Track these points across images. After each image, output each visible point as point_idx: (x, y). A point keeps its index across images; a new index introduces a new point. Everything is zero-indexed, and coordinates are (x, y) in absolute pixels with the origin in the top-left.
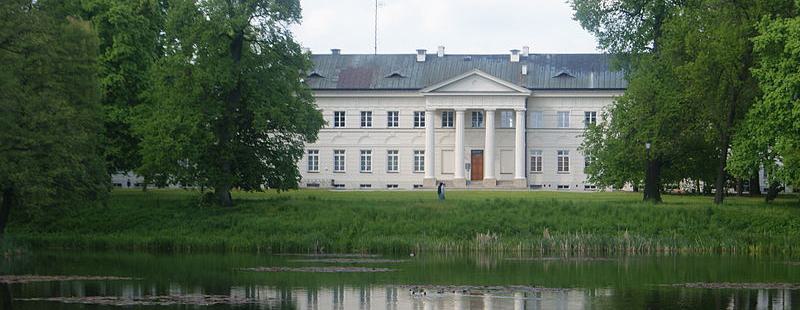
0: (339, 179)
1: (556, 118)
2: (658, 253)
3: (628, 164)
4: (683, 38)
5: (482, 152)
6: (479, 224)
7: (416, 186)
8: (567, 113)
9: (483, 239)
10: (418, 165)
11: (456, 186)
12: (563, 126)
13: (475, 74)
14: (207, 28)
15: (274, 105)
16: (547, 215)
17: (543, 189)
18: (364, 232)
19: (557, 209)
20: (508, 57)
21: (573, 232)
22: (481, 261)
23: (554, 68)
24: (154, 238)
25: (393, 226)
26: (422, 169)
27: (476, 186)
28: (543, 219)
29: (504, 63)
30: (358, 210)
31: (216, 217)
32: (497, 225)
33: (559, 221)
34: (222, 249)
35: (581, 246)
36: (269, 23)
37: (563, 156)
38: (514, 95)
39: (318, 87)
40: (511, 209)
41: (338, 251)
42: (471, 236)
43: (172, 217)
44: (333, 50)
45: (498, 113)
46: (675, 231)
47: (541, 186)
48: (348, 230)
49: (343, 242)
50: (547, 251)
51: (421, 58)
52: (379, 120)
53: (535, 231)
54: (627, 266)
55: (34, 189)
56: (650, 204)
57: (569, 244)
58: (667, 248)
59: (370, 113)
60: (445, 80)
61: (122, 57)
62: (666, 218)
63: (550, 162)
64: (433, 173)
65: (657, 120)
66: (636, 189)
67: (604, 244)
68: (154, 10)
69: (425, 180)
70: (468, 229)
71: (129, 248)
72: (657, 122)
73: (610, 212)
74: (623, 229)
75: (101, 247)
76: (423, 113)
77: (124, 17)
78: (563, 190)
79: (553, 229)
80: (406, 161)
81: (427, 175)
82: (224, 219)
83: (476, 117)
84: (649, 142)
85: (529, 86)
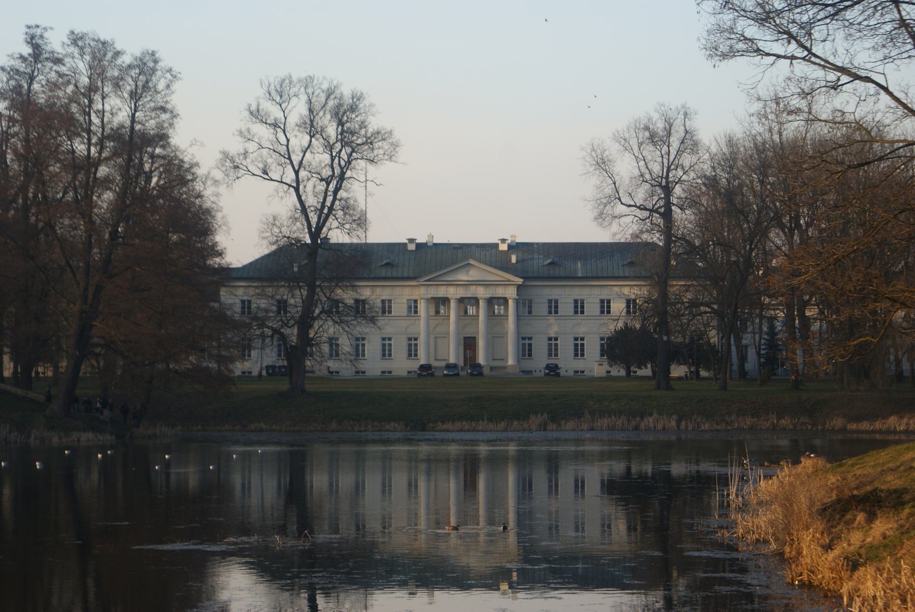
5: (474, 338)
10: (412, 352)
13: (469, 264)
20: (496, 245)
23: (541, 256)
26: (416, 355)
37: (527, 342)
38: (506, 284)
39: (399, 275)
59: (390, 301)
76: (416, 301)
77: (600, 188)
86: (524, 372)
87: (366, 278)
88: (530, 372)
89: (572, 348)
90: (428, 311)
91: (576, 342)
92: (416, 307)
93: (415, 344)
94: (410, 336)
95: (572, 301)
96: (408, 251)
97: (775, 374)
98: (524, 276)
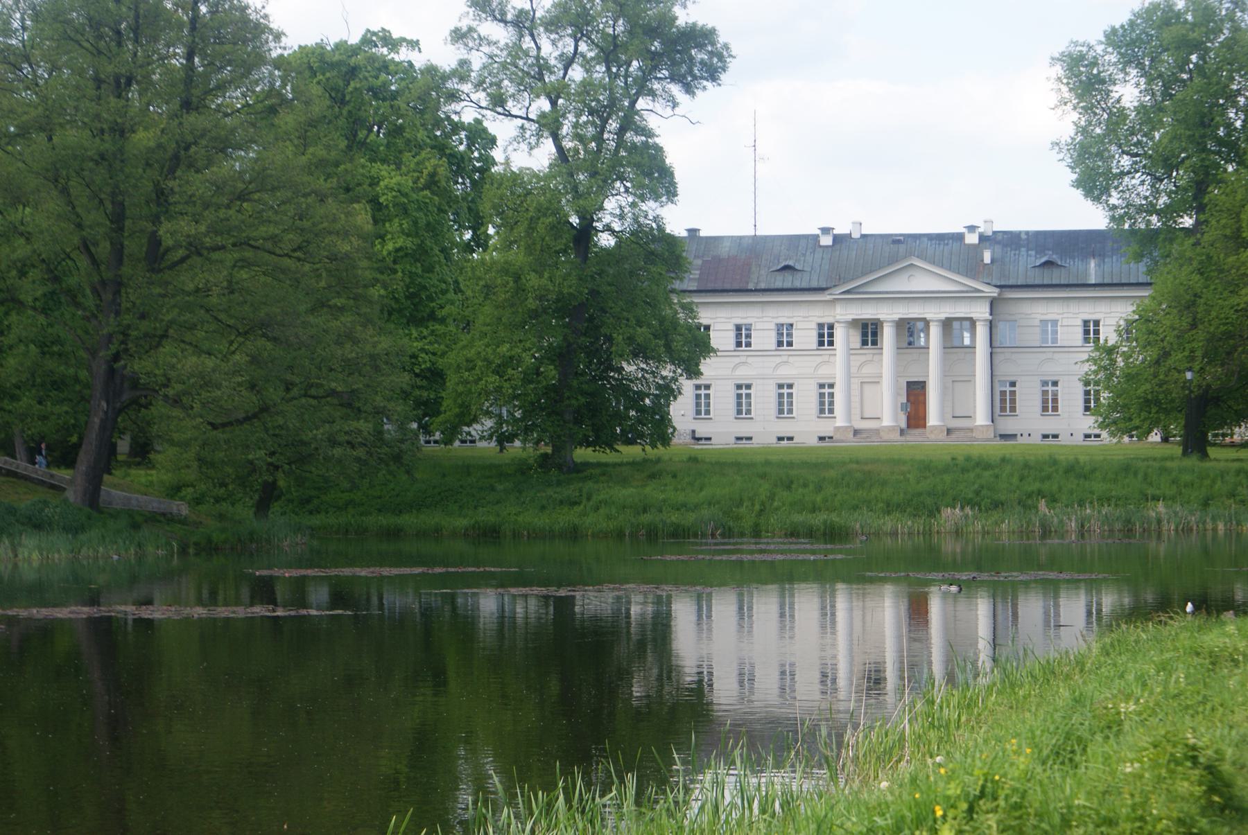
0: (702, 429)
1: (1038, 330)
2: (1210, 534)
3: (1157, 402)
4: (1238, 214)
6: (944, 494)
7: (821, 439)
8: (1055, 322)
9: (950, 515)
10: (825, 405)
11: (885, 436)
12: (1049, 342)
14: (545, 215)
15: (640, 323)
16: (1042, 480)
17: (1020, 440)
18: (777, 509)
19: (1057, 471)
20: (959, 237)
21: (1081, 504)
22: (949, 546)
23: (1033, 253)
24: (473, 521)
25: (819, 499)
26: (831, 411)
27: (915, 436)
28: (1037, 486)
29: (956, 246)
30: (763, 476)
31: (559, 489)
32: (971, 495)
33: (1060, 489)
34: (573, 534)
35: (1095, 526)
36: (633, 205)
39: (804, 285)
40: (991, 472)
41: (742, 535)
42: (934, 512)
43: (493, 489)
44: (689, 231)
45: (947, 324)
46: (1232, 501)
47: (1015, 436)
48: (753, 505)
49: (748, 523)
50: (1046, 532)
51: (826, 241)
52: (764, 338)
53: (1026, 503)
54: (1162, 554)
55: (337, 452)
56: (1193, 461)
57: (1076, 521)
58: (1221, 526)
60: (864, 274)
61: (400, 254)
62: (1219, 483)
63: (1028, 399)
64: (849, 418)
65: (1201, 335)
66: (1165, 440)
67: (1128, 521)
68: (443, 183)
69: (837, 429)
70: (929, 501)
71: (436, 533)
72: (1199, 340)
73: (1136, 474)
74: (1156, 498)
75: (394, 534)
76: (831, 327)
78: (1050, 441)
79: (1053, 500)
80: (805, 399)
81: (840, 421)
82: (569, 491)
83: (909, 330)
84: (1190, 369)
85: (995, 282)
86: (1004, 437)
87: (751, 291)
88: (1013, 436)
90: (848, 342)
92: (831, 335)
94: (822, 381)
95: (1080, 323)
96: (821, 246)
98: (1003, 283)
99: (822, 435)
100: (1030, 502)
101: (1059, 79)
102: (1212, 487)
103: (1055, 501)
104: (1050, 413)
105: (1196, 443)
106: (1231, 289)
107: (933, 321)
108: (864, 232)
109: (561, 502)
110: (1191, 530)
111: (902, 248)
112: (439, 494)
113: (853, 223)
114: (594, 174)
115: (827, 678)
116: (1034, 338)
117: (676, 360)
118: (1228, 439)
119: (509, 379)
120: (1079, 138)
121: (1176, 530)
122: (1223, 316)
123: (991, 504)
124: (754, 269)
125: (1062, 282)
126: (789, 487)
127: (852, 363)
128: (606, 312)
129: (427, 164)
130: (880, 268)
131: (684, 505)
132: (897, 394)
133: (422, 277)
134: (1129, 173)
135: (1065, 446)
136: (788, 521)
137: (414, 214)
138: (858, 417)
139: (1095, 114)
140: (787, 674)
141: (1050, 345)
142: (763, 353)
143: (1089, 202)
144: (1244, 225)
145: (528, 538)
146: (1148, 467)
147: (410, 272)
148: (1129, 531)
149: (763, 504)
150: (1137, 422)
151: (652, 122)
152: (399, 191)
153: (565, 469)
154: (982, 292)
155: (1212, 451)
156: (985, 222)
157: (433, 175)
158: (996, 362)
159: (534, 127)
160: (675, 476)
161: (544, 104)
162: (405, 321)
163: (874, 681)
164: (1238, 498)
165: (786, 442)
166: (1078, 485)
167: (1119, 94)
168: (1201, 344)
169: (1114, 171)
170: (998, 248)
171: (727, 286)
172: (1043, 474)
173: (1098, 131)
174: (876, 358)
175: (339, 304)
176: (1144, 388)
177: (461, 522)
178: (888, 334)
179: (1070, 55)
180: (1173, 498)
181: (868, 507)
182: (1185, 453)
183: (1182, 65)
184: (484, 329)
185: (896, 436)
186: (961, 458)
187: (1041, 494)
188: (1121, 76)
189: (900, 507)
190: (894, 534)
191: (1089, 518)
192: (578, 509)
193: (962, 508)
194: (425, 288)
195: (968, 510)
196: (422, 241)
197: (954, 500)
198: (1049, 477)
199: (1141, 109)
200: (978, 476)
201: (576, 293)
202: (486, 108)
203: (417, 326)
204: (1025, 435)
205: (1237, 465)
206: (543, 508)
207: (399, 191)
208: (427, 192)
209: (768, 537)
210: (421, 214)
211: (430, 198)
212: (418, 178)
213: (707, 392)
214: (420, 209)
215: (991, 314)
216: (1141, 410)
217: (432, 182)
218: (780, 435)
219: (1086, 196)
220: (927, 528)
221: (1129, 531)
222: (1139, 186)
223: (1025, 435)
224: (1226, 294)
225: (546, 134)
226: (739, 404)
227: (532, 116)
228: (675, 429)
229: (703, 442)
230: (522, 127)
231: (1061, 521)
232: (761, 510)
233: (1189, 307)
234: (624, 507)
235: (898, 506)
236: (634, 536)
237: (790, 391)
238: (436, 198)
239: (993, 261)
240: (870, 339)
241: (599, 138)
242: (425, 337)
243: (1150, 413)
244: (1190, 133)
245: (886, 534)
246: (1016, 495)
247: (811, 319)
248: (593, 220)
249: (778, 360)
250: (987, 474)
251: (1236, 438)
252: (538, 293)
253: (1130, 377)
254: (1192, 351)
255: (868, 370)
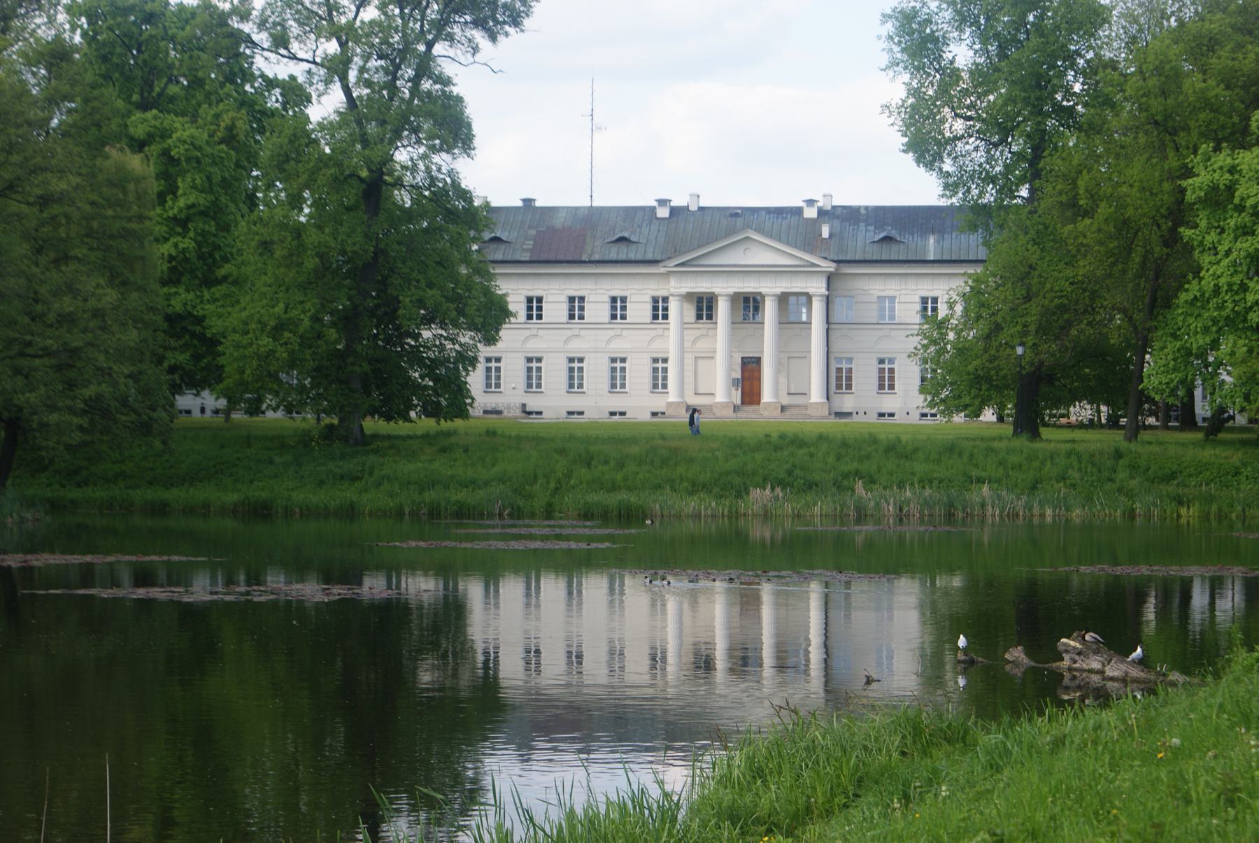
0: (533, 403)
1: (875, 306)
3: (989, 379)
4: (1074, 182)
7: (654, 414)
9: (759, 497)
10: (658, 381)
11: (719, 413)
12: (886, 319)
13: (748, 238)
14: (326, 166)
15: (430, 285)
16: (861, 460)
17: (855, 418)
20: (799, 211)
21: (901, 486)
22: (759, 532)
25: (619, 477)
26: (665, 386)
27: (749, 413)
29: (794, 219)
30: (562, 452)
31: (340, 463)
34: (350, 512)
35: (914, 509)
36: (424, 157)
37: (886, 366)
39: (639, 257)
41: (532, 515)
42: (741, 492)
43: (271, 462)
44: (524, 200)
45: (783, 299)
48: (548, 483)
49: (539, 503)
50: (861, 517)
51: (663, 213)
52: (597, 310)
53: (841, 485)
54: (986, 540)
56: (1023, 442)
57: (895, 504)
58: (1049, 512)
59: (582, 299)
60: (699, 246)
61: (192, 211)
62: (1048, 464)
63: (865, 377)
64: (681, 392)
65: (1034, 309)
66: (1001, 419)
67: (951, 505)
69: (669, 404)
70: (737, 481)
71: (204, 510)
73: (960, 455)
74: (980, 481)
75: (160, 509)
76: (665, 299)
78: (887, 420)
79: (871, 481)
80: (638, 373)
81: (673, 396)
82: (350, 465)
83: (749, 305)
86: (839, 415)
87: (585, 262)
89: (875, 375)
90: (682, 315)
91: (882, 366)
92: (666, 309)
93: (496, 368)
96: (657, 219)
97: (1091, 421)
98: (840, 258)
99: (655, 410)
100: (846, 483)
101: (891, 38)
102: (1040, 469)
103: (873, 482)
104: (886, 391)
105: (1028, 423)
106: (1067, 260)
107: (768, 295)
108: (702, 205)
109: (342, 477)
110: (1018, 515)
111: (740, 221)
112: (214, 466)
113: (691, 195)
114: (383, 123)
115: (657, 659)
116: (871, 314)
117: (472, 326)
118: (1063, 421)
119: (286, 343)
120: (911, 100)
121: (1001, 516)
122: (1057, 288)
123: (804, 484)
124: (588, 240)
125: (901, 258)
126: (589, 465)
127: (686, 338)
128: (394, 272)
129: (225, 116)
130: (717, 240)
131: (473, 482)
132: (730, 369)
133: (215, 236)
134: (962, 137)
135: (899, 425)
136: (582, 501)
137: (208, 168)
138: (692, 392)
139: (929, 75)
140: (616, 654)
141: (887, 321)
142: (596, 325)
143: (922, 169)
144: (1081, 192)
145: (301, 516)
146: (974, 447)
147: (203, 231)
148: (950, 517)
149: (559, 481)
150: (967, 400)
151: (448, 68)
152: (192, 144)
153: (352, 441)
154: (820, 266)
155: (1045, 432)
156: (824, 196)
157: (230, 128)
158: (832, 338)
159: (322, 71)
160: (466, 450)
161: (332, 47)
162: (197, 282)
163: (704, 664)
164: (1069, 482)
165: (618, 416)
166: (898, 465)
167: (953, 54)
168: (1034, 318)
169: (948, 134)
170: (837, 223)
171: (561, 258)
172: (863, 453)
173: (931, 92)
174: (711, 332)
175: (79, 255)
176: (975, 363)
177: (232, 498)
178: (722, 309)
179: (901, 12)
180: (999, 481)
181: (671, 487)
182: (1015, 433)
183: (1021, 22)
184: (263, 289)
185: (729, 413)
186: (775, 435)
187: (858, 474)
188: (956, 34)
189: (706, 487)
190: (697, 516)
191: (908, 502)
192: (358, 484)
193: (773, 489)
194: (219, 248)
195: (778, 490)
196: (217, 198)
197: (765, 480)
198: (868, 457)
199: (976, 71)
200: (793, 455)
201: (361, 252)
202: (268, 50)
203: (209, 288)
204: (861, 413)
205: (1068, 446)
206: (321, 483)
207: (192, 144)
208: (223, 147)
209: (561, 518)
210: (216, 169)
211: (226, 153)
212: (215, 132)
213: (539, 365)
214: (214, 163)
215: (828, 290)
216: (971, 387)
217: (230, 138)
218: (570, 410)
219: (918, 161)
220: (734, 510)
221: (950, 517)
222: (974, 152)
223: (861, 413)
224: (1061, 265)
225: (336, 78)
226: (571, 378)
227: (318, 60)
228: (473, 399)
229: (534, 416)
230: (309, 72)
231: (877, 504)
232: (557, 489)
233: (1022, 280)
234: (409, 483)
235: (704, 486)
236: (415, 515)
237: (623, 365)
238: (233, 153)
239: (831, 236)
240: (705, 313)
241: (392, 87)
242: (217, 300)
243: (980, 390)
244: (1026, 94)
245: (688, 516)
246: (832, 475)
247: (645, 292)
248: (383, 174)
249: (611, 333)
250: (802, 452)
251: (1073, 419)
252: (317, 250)
253: (962, 351)
254: (1025, 326)
255: (702, 345)
